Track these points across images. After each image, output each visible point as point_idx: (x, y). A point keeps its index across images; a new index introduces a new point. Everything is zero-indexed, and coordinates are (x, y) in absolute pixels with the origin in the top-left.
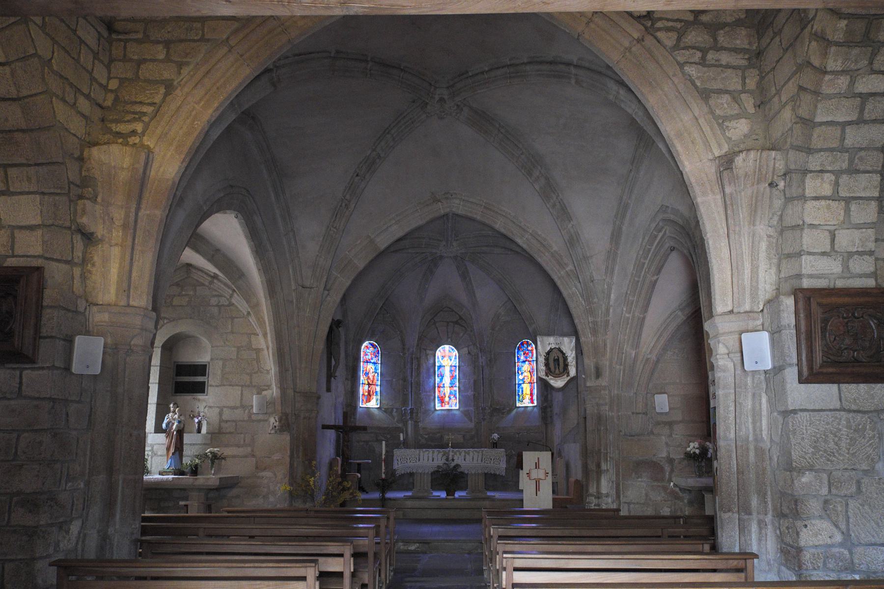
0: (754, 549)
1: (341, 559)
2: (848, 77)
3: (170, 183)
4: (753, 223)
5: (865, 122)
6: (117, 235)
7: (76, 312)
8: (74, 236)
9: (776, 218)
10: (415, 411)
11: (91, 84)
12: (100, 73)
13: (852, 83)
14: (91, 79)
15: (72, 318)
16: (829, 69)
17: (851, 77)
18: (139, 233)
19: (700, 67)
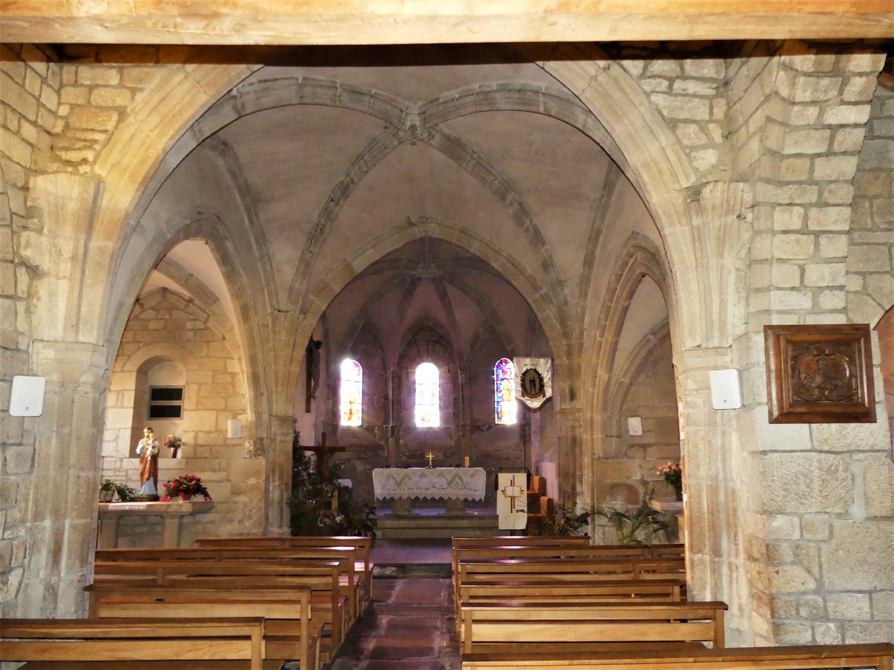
0: (725, 600)
1: (298, 607)
2: (818, 108)
3: (123, 213)
4: (721, 255)
5: (835, 154)
6: (66, 267)
7: (18, 350)
8: (17, 270)
9: (744, 251)
10: (396, 429)
11: (38, 111)
12: (49, 98)
13: (821, 114)
14: (38, 105)
15: (12, 357)
16: (797, 100)
17: (820, 108)
18: (90, 266)
19: (667, 96)
